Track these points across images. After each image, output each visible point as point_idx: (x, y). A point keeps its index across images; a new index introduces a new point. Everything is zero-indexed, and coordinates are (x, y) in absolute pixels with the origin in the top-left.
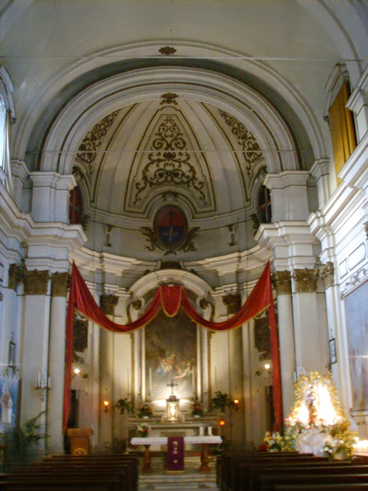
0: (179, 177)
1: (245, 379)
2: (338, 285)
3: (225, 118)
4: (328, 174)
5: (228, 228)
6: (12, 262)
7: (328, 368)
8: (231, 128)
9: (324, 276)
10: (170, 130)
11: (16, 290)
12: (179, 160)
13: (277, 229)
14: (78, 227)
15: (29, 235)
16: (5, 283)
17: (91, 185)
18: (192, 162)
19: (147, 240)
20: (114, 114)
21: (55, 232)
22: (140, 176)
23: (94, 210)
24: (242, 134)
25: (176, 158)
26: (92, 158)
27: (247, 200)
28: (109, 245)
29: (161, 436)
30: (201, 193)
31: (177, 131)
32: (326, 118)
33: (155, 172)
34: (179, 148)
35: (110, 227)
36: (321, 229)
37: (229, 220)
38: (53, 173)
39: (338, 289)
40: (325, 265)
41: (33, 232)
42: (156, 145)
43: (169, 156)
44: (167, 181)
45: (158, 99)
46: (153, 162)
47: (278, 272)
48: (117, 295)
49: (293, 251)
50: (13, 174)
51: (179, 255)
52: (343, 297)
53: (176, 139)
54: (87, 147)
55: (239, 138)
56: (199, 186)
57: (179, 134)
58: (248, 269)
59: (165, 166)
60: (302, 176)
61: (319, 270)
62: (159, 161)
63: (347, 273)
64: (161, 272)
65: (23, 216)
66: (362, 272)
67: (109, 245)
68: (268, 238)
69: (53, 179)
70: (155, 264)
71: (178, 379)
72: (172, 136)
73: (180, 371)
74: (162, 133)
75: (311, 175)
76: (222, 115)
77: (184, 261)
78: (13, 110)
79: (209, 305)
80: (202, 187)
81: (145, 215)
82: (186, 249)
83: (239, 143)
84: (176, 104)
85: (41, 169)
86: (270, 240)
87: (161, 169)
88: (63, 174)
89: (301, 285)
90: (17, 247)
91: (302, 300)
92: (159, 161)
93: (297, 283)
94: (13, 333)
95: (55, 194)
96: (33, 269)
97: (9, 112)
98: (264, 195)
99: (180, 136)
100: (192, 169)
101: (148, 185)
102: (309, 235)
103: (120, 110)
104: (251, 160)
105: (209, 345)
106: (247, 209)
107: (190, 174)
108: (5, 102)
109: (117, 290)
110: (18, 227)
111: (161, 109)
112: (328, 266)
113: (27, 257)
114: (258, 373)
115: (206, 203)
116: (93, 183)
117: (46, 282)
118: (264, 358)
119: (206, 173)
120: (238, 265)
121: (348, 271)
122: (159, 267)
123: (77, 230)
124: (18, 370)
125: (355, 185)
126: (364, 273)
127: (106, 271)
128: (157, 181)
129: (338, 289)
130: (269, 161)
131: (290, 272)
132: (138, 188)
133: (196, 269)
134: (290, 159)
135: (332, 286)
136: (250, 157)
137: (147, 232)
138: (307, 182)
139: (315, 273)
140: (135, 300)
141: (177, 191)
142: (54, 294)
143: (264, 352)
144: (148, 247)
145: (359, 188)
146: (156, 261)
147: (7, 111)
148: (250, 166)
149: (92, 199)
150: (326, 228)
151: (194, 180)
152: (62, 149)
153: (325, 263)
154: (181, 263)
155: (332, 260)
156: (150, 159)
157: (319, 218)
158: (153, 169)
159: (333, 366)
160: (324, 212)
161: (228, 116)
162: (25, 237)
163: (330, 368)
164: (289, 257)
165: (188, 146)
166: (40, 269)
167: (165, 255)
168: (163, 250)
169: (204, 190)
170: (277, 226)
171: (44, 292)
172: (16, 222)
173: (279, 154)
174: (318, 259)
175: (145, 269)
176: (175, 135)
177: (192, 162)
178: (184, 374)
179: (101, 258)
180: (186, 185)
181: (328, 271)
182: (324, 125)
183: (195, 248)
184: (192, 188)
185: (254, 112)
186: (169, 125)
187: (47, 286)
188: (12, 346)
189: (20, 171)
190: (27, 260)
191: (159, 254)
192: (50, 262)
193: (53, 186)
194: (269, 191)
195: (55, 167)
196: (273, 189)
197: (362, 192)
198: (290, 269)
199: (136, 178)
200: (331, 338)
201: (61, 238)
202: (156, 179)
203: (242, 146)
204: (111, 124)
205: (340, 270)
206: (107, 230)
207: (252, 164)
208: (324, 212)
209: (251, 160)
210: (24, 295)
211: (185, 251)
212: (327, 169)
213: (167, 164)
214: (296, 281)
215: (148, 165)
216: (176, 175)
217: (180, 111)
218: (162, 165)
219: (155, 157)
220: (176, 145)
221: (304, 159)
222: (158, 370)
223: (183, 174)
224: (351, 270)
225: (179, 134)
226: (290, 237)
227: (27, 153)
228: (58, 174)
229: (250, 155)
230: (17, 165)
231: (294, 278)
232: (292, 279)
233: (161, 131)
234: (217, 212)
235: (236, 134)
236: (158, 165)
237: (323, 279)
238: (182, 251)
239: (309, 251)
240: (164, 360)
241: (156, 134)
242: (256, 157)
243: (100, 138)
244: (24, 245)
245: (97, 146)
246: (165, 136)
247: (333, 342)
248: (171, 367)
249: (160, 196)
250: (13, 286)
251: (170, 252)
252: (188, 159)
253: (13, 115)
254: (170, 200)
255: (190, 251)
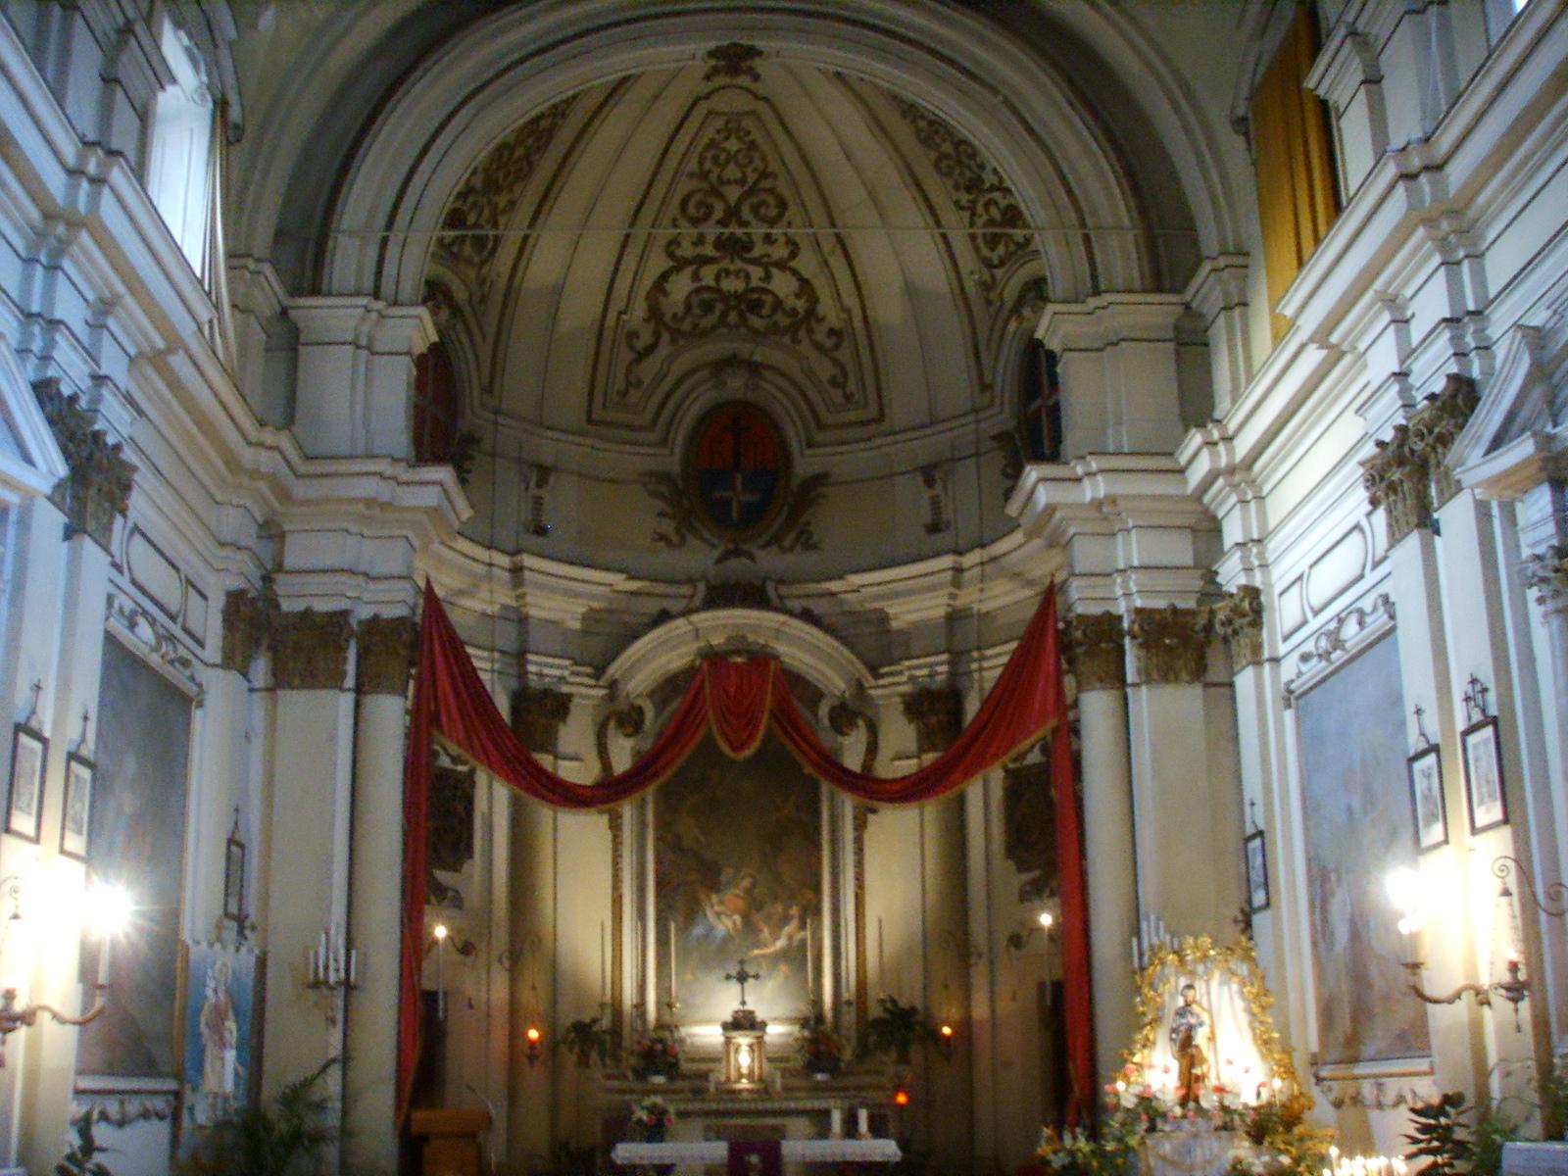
0: (765, 312)
1: (973, 960)
2: (1275, 660)
3: (913, 121)
4: (1244, 304)
5: (920, 479)
6: (235, 583)
7: (1242, 925)
8: (933, 155)
9: (1229, 630)
10: (736, 162)
11: (245, 674)
12: (766, 259)
13: (1079, 480)
14: (444, 474)
15: (285, 496)
16: (213, 651)
17: (484, 337)
18: (806, 264)
19: (661, 514)
20: (559, 112)
21: (368, 488)
22: (640, 309)
23: (491, 416)
24: (968, 174)
25: (756, 252)
26: (486, 253)
27: (985, 388)
28: (541, 531)
29: (707, 1140)
30: (836, 362)
31: (757, 163)
32: (1240, 124)
33: (689, 296)
34: (765, 220)
35: (544, 473)
36: (1220, 482)
37: (925, 447)
38: (363, 301)
39: (1275, 674)
40: (1232, 596)
41: (300, 489)
42: (691, 210)
43: (734, 247)
44: (728, 325)
45: (698, 62)
46: (680, 264)
47: (1079, 616)
48: (566, 689)
49: (1132, 549)
50: (234, 306)
51: (769, 561)
52: (1290, 697)
53: (752, 191)
54: (471, 219)
55: (957, 187)
56: (829, 343)
57: (764, 175)
58: (985, 607)
59: (718, 278)
60: (1157, 312)
61: (1212, 613)
62: (704, 261)
63: (1305, 623)
64: (703, 618)
65: (269, 437)
66: (1354, 619)
67: (541, 531)
68: (1051, 509)
69: (363, 319)
70: (686, 590)
71: (763, 956)
72: (742, 182)
73: (766, 932)
74: (709, 171)
75: (1187, 307)
76: (904, 114)
77: (781, 581)
78: (233, 98)
79: (861, 723)
80: (837, 346)
81: (654, 436)
82: (787, 543)
83: (956, 203)
84: (756, 78)
85: (325, 288)
86: (1058, 515)
87: (708, 288)
88: (395, 303)
89: (1154, 660)
90: (249, 536)
91: (1161, 709)
92: (704, 261)
93: (1142, 653)
94: (237, 810)
95: (369, 369)
96: (299, 606)
97: (221, 106)
98: (1038, 371)
99: (767, 184)
100: (805, 285)
101: (666, 337)
102: (1185, 498)
103: (574, 97)
104: (996, 261)
105: (859, 851)
106: (982, 415)
107: (800, 305)
108: (209, 75)
109: (566, 673)
110: (255, 474)
111: (707, 97)
112: (1242, 600)
113: (279, 567)
114: (1016, 941)
115: (848, 398)
116: (490, 339)
117: (341, 649)
118: (1034, 892)
119: (850, 300)
120: (953, 596)
121: (1309, 615)
122: (697, 602)
123: (441, 484)
124: (253, 928)
125: (1334, 338)
126: (1361, 623)
127: (533, 612)
128: (695, 326)
129: (1275, 674)
130: (1056, 258)
131: (1120, 618)
132: (632, 348)
133: (819, 607)
134: (1121, 254)
135: (1257, 663)
136: (992, 250)
137: (664, 489)
138: (1177, 328)
139: (1202, 621)
140: (621, 705)
141: (758, 358)
142: (366, 688)
143: (1037, 873)
144: (662, 537)
145: (1344, 347)
146: (691, 581)
147: (215, 102)
148: (993, 277)
149: (486, 381)
150: (1237, 478)
151: (813, 322)
152: (390, 224)
153: (1234, 590)
154: (770, 588)
155: (1257, 581)
156: (671, 255)
157: (1215, 444)
158: (681, 287)
159: (1258, 920)
160: (1232, 426)
161: (922, 117)
162: (276, 504)
163: (1247, 926)
164: (1118, 571)
165: (793, 212)
166: (321, 606)
167: (719, 561)
168: (714, 546)
169: (844, 355)
170: (1080, 470)
171: (335, 682)
172: (248, 456)
173: (1087, 239)
174: (1211, 576)
175: (653, 606)
176: (752, 178)
177: (806, 264)
178: (781, 943)
179: (517, 571)
180: (787, 340)
181: (1243, 615)
182: (1234, 147)
183: (816, 538)
184: (805, 347)
185: (1006, 102)
186: (733, 145)
187: (345, 660)
188: (235, 849)
189: (257, 293)
190: (280, 578)
191: (700, 557)
192: (352, 586)
193: (363, 342)
194: (1052, 358)
195: (368, 283)
196: (1065, 350)
197: (1355, 362)
198: (1121, 608)
199: (625, 317)
200: (1250, 830)
201: (385, 506)
202: (689, 319)
203: (966, 214)
204: (546, 145)
205: (1283, 611)
206: (533, 484)
207: (998, 272)
208: (1232, 426)
209: (996, 261)
210: (271, 690)
211: (784, 550)
212: (1243, 290)
213: (727, 272)
214: (1141, 646)
215: (664, 277)
216: (755, 307)
217: (766, 100)
218: (708, 274)
219: (687, 250)
220: (755, 209)
221: (1169, 252)
222: (698, 930)
223: (778, 304)
224: (1316, 613)
225: (764, 175)
226: (1122, 505)
227: (280, 235)
228: (380, 305)
229: (993, 241)
230: (247, 275)
231: (1134, 637)
232: (1127, 641)
233: (708, 165)
234: (884, 427)
235: (949, 175)
236: (696, 277)
237: (1226, 640)
238: (774, 549)
239: (1179, 550)
240: (715, 898)
241: (691, 175)
242: (1012, 248)
243: (511, 188)
244: (272, 531)
245: (504, 211)
246: (720, 178)
247: (1257, 842)
248: (737, 918)
249: (705, 373)
250: (239, 659)
251: (737, 553)
252: (793, 255)
253: (235, 114)
254: (735, 385)
255: (798, 548)
